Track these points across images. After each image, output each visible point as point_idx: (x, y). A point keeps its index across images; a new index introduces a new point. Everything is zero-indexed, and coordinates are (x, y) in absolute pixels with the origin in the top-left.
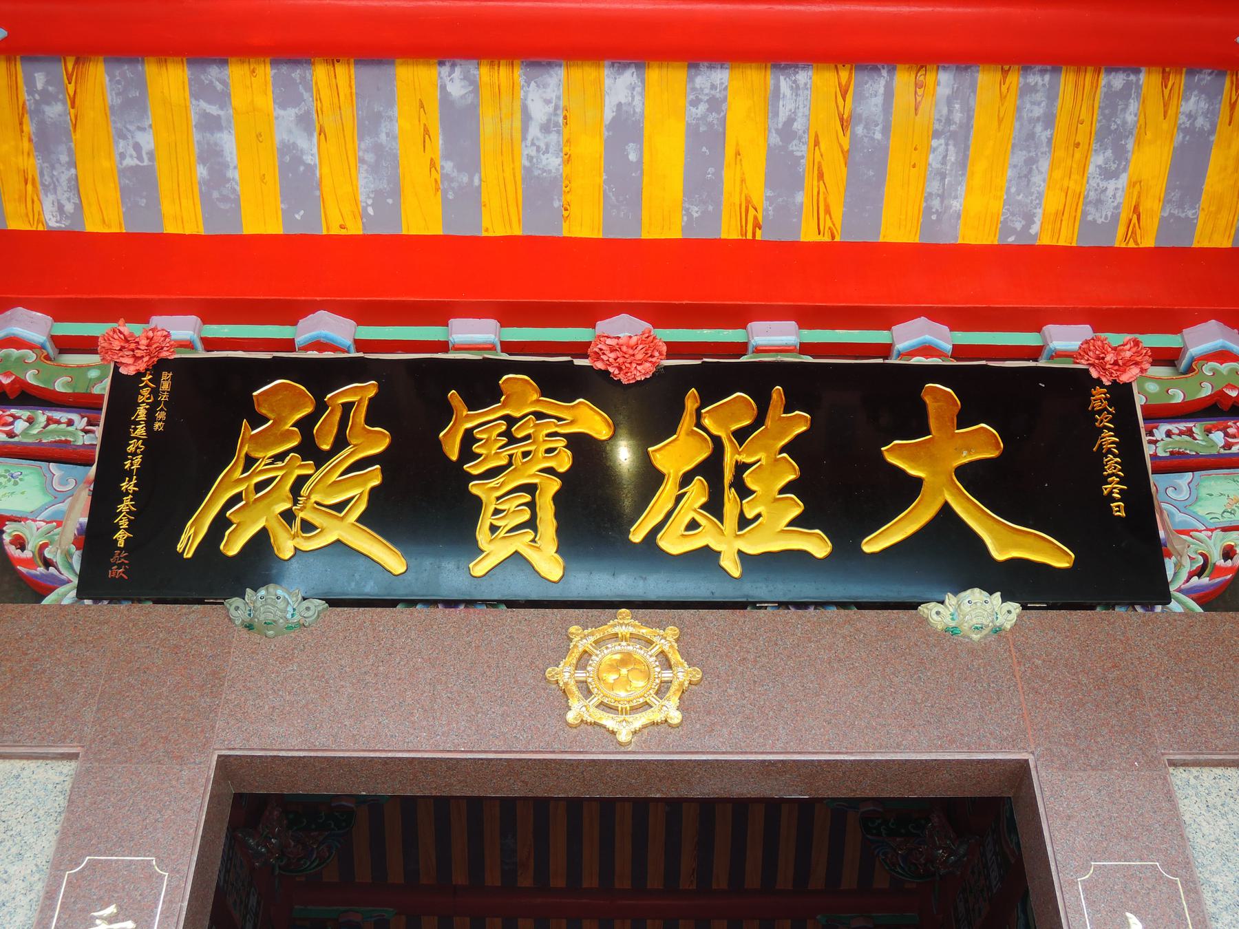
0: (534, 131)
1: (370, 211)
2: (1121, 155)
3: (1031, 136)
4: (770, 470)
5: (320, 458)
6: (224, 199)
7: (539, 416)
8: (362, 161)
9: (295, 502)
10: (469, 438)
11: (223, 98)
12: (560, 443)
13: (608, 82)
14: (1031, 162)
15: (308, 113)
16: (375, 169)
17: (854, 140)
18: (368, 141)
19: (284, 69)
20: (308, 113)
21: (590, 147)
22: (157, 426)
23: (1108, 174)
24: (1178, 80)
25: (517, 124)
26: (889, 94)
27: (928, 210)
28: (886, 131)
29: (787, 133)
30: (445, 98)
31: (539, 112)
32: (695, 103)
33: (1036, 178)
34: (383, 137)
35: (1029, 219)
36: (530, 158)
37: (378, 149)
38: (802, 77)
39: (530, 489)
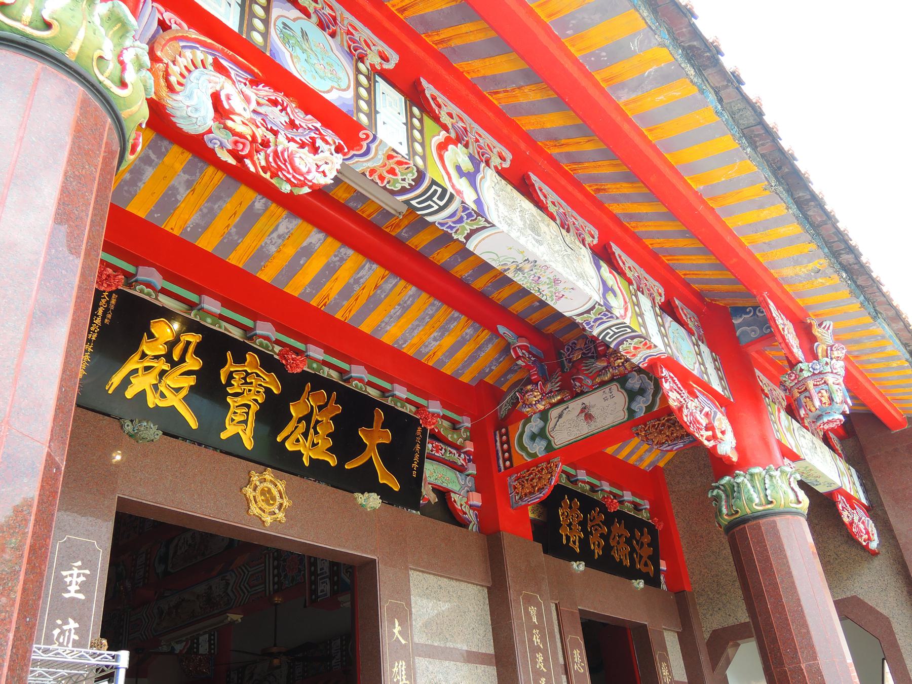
0: (275, 235)
1: (189, 229)
2: (442, 336)
3: (424, 318)
4: (326, 426)
5: (174, 364)
6: (128, 192)
7: (258, 375)
8: (201, 210)
9: (160, 382)
10: (230, 376)
11: (161, 155)
12: (262, 390)
13: (313, 233)
14: (418, 326)
15: (193, 181)
16: (203, 216)
17: (375, 294)
18: (209, 204)
19: (196, 160)
20: (193, 181)
21: (290, 251)
22: (106, 321)
23: (435, 340)
24: (471, 322)
25: (271, 230)
26: (395, 285)
27: (379, 326)
28: (386, 296)
29: (357, 281)
30: (252, 206)
31: (282, 229)
32: (335, 256)
33: (416, 331)
34: (217, 206)
35: (405, 341)
36: (266, 243)
37: (211, 210)
38: (375, 266)
39: (248, 406)
